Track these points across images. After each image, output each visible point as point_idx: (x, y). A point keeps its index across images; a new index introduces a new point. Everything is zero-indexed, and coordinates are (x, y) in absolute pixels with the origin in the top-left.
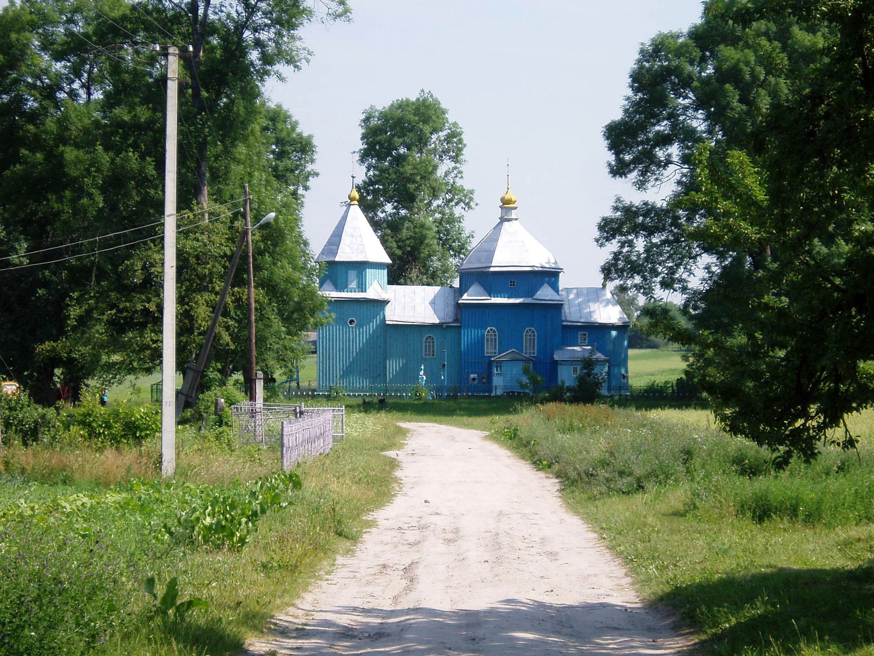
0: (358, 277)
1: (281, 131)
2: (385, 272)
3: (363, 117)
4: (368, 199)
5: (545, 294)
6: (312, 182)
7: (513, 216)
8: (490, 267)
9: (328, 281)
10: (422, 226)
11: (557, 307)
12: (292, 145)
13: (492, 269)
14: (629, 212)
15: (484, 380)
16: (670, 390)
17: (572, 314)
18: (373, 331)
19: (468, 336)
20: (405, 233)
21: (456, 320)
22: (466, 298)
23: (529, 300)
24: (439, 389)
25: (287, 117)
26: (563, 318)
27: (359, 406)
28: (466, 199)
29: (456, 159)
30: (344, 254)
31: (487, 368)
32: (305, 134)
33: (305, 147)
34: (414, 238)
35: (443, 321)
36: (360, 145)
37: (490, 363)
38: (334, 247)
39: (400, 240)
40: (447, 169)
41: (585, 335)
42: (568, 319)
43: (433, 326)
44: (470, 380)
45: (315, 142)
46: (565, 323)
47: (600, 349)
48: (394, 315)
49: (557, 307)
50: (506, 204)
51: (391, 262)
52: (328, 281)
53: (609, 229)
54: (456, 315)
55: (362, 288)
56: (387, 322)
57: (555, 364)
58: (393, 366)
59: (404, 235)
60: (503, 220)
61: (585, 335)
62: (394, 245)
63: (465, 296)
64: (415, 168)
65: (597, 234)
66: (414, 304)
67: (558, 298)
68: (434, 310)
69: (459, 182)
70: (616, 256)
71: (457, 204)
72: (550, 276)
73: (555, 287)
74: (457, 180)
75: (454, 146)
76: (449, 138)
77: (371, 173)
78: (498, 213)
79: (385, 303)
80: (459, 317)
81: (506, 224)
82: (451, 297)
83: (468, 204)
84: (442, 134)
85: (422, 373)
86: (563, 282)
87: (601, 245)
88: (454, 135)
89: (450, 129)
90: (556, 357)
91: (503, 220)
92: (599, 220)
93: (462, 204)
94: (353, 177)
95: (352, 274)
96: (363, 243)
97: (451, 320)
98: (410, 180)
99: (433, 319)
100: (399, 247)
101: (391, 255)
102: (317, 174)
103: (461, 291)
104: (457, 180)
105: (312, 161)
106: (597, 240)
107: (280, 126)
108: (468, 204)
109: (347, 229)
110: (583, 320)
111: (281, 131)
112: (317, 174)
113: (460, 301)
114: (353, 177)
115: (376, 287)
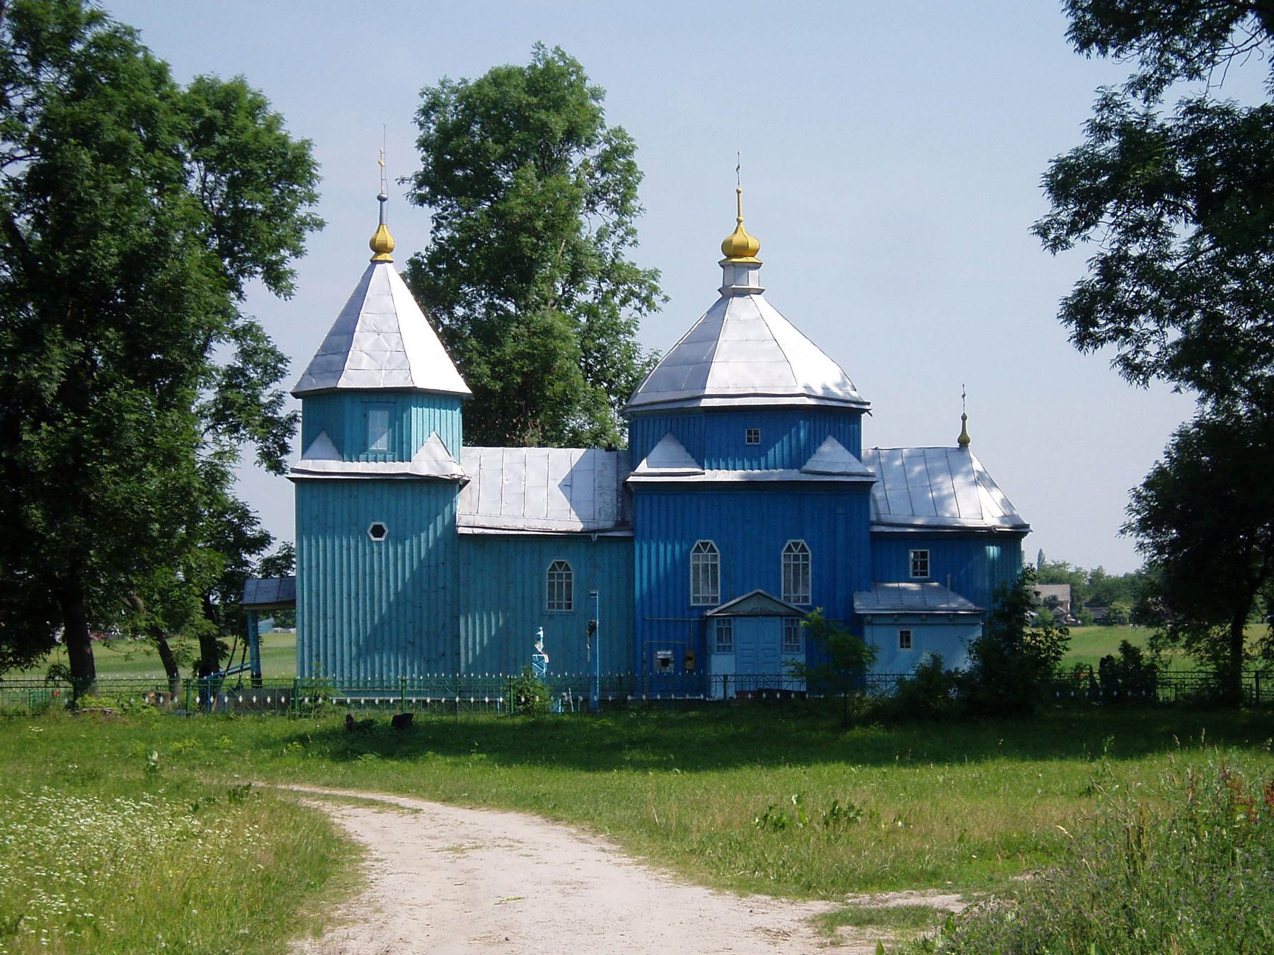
0: (391, 425)
1: (243, 129)
2: (455, 417)
3: (422, 102)
4: (432, 284)
5: (831, 458)
6: (310, 239)
7: (753, 285)
8: (700, 398)
9: (323, 436)
10: (548, 332)
11: (860, 490)
12: (263, 159)
13: (705, 403)
14: (1139, 144)
15: (689, 665)
16: (1085, 684)
17: (894, 506)
18: (429, 551)
19: (651, 560)
20: (509, 348)
21: (621, 524)
22: (646, 471)
23: (794, 475)
24: (582, 687)
25: (257, 106)
26: (873, 518)
27: (325, 736)
28: (644, 289)
29: (621, 207)
30: (360, 372)
31: (699, 636)
32: (295, 139)
33: (293, 167)
34: (531, 357)
35: (592, 526)
36: (416, 162)
37: (704, 622)
38: (337, 358)
39: (500, 362)
40: (602, 224)
41: (924, 555)
42: (884, 518)
43: (568, 538)
44: (656, 664)
45: (315, 155)
46: (877, 529)
47: (959, 588)
48: (475, 512)
49: (860, 490)
50: (736, 257)
51: (468, 391)
52: (323, 436)
53: (1079, 188)
54: (621, 512)
55: (401, 450)
56: (461, 530)
57: (857, 623)
58: (476, 632)
59: (508, 351)
60: (729, 293)
61: (924, 555)
62: (486, 369)
63: (643, 467)
64: (531, 203)
65: (1043, 206)
66: (524, 490)
67: (856, 467)
68: (570, 501)
69: (629, 255)
70: (1110, 268)
71: (624, 302)
72: (840, 418)
73: (852, 444)
74: (625, 249)
75: (618, 175)
76: (605, 163)
77: (445, 234)
78: (717, 277)
79: (454, 485)
80: (629, 518)
81: (736, 302)
82: (610, 473)
83: (647, 301)
84: (593, 153)
85: (540, 646)
86: (872, 434)
87: (1058, 244)
88: (618, 159)
89: (608, 141)
90: (861, 605)
91: (729, 293)
92: (1048, 168)
93: (635, 302)
94: (382, 199)
95: (378, 418)
96: (409, 349)
97: (609, 524)
98: (524, 226)
99: (567, 520)
100: (495, 376)
101: (468, 377)
102: (320, 225)
103: (632, 458)
104: (625, 249)
105: (312, 199)
106: (1043, 231)
107: (240, 120)
108: (647, 301)
109: (367, 317)
110: (919, 522)
111: (243, 129)
112: (320, 225)
113: (630, 479)
114: (382, 199)
115: (435, 448)
